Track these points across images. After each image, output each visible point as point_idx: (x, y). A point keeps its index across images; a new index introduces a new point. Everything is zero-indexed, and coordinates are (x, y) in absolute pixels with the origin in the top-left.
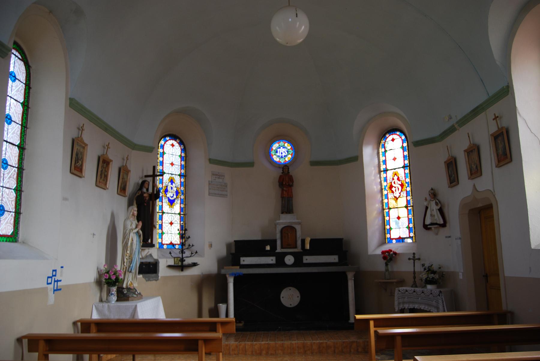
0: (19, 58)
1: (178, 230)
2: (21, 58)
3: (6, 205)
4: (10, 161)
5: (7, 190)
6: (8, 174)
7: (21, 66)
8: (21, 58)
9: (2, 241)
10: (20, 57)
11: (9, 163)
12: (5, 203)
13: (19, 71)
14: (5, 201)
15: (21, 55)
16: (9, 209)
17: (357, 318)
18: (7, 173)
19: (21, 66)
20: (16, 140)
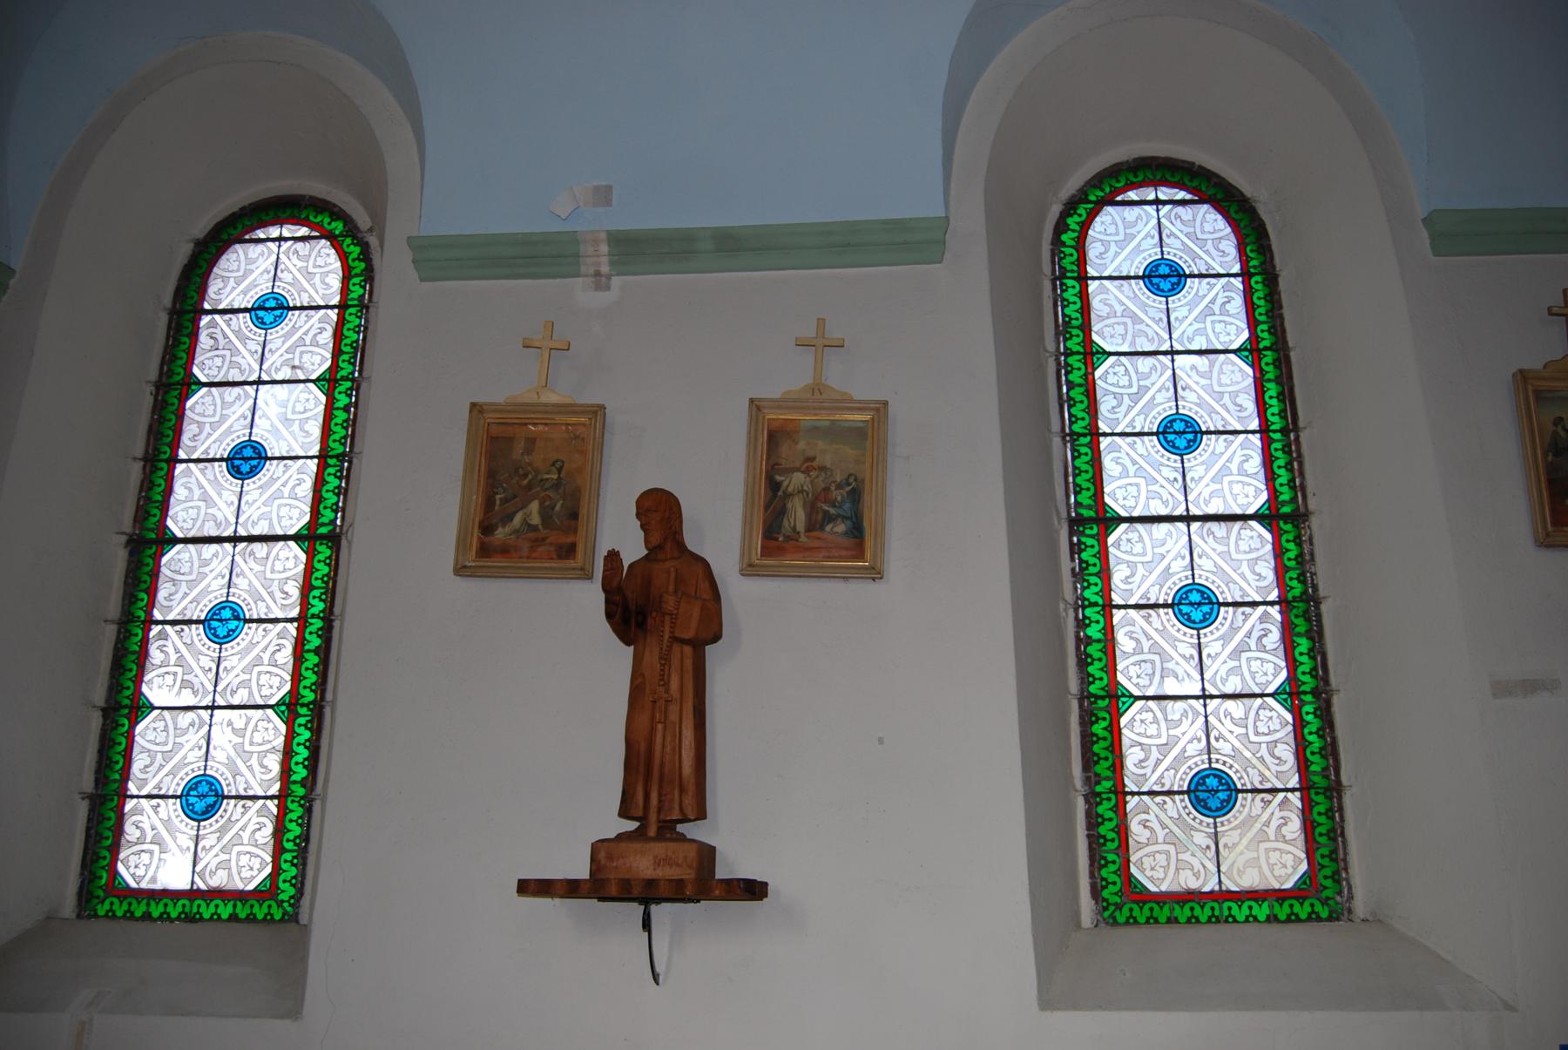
0: (1183, 203)
1: (151, 394)
2: (1189, 197)
3: (1223, 630)
4: (1157, 457)
5: (1230, 705)
6: (1226, 639)
7: (227, 274)
8: (1189, 197)
9: (1147, 922)
10: (304, 231)
11: (1167, 616)
12: (1193, 828)
13: (553, 422)
14: (1152, 312)
15: (1182, 187)
16: (245, 790)
17: (203, 317)
18: (1222, 638)
19: (227, 274)
20: (184, 514)
